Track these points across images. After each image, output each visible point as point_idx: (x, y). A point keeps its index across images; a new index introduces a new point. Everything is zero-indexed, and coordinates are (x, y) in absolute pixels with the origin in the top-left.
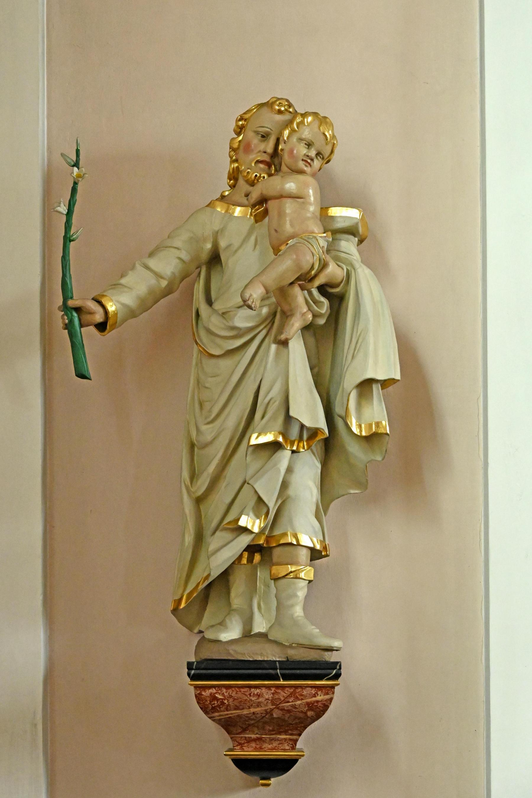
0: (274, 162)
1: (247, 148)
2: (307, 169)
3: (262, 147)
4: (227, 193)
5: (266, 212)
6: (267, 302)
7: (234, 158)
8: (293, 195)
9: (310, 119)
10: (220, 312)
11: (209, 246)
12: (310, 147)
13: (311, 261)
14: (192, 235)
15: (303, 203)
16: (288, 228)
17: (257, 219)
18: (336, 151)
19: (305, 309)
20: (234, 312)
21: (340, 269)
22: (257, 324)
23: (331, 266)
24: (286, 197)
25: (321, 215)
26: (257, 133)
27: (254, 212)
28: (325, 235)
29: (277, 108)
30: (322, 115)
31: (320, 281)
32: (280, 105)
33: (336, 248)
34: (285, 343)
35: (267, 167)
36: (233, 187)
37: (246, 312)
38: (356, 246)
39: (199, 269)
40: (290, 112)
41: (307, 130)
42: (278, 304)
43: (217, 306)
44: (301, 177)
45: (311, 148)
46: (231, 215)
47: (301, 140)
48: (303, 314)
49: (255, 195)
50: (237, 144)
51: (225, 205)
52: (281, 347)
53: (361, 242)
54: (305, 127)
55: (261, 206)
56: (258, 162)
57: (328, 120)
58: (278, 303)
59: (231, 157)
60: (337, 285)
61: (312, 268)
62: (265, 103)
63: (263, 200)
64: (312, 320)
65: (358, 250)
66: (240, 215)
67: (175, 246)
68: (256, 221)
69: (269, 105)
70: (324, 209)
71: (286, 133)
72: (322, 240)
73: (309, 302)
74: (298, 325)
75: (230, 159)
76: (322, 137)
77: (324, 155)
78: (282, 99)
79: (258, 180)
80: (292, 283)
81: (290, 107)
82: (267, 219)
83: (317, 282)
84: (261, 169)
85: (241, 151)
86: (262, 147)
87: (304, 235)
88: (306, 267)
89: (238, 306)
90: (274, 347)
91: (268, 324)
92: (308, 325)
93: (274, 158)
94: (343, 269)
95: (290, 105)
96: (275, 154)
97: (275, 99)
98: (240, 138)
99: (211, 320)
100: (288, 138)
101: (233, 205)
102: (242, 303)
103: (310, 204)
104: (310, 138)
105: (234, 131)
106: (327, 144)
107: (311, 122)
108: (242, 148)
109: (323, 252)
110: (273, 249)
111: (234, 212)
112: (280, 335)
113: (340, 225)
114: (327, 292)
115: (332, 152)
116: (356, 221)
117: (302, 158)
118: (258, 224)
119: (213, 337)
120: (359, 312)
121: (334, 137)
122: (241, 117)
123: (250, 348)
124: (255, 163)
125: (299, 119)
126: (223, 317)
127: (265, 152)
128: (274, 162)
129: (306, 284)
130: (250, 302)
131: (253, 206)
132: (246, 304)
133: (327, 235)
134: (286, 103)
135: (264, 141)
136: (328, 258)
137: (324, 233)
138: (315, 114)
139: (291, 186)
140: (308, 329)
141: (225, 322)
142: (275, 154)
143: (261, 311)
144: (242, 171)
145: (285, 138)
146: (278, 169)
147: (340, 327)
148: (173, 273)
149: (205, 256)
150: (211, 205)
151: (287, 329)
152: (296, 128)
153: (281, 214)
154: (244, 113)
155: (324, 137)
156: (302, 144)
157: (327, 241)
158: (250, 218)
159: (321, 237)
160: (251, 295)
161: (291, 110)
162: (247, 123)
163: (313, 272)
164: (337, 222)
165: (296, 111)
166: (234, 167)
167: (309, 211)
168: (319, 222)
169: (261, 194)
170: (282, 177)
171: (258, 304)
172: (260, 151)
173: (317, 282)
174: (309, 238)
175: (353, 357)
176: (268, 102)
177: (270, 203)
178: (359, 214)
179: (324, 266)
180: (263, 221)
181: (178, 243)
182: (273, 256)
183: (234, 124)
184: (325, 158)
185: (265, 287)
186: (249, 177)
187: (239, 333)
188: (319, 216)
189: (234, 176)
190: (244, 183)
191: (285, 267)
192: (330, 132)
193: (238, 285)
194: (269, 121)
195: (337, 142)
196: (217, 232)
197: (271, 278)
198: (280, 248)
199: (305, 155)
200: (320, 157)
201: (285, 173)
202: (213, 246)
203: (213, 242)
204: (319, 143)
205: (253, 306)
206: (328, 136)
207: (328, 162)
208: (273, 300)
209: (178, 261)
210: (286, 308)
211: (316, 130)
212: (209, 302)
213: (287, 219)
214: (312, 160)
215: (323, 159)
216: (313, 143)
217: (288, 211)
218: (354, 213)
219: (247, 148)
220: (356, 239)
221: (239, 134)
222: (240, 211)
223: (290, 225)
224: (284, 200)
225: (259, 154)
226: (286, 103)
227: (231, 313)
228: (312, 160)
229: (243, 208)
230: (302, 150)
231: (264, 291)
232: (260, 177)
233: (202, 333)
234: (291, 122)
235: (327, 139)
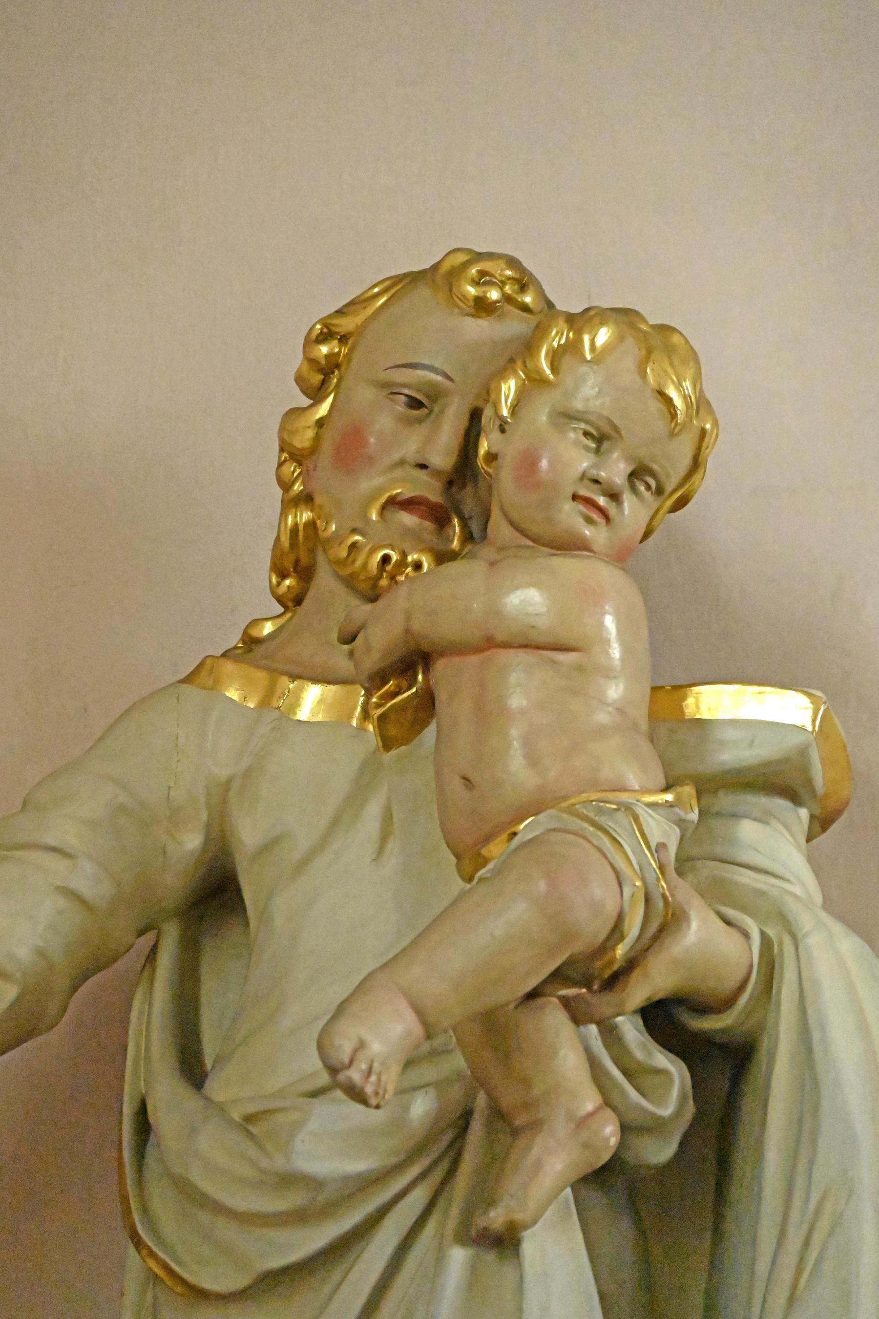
0: (459, 502)
1: (349, 447)
2: (596, 534)
3: (411, 445)
4: (268, 628)
5: (427, 705)
6: (429, 1072)
7: (298, 487)
8: (541, 639)
9: (603, 335)
10: (236, 1115)
11: (192, 841)
12: (606, 445)
13: (611, 908)
14: (123, 798)
15: (580, 668)
16: (518, 770)
17: (392, 731)
18: (712, 462)
19: (590, 1101)
20: (294, 1116)
21: (737, 936)
22: (394, 1160)
23: (694, 925)
24: (506, 645)
25: (653, 716)
26: (390, 389)
27: (378, 706)
28: (669, 797)
29: (472, 291)
30: (652, 322)
31: (654, 982)
32: (483, 279)
33: (719, 850)
34: (505, 1242)
35: (429, 525)
36: (293, 602)
37: (342, 1112)
38: (803, 840)
39: (150, 936)
40: (525, 308)
41: (591, 380)
42: (478, 1080)
43: (215, 1088)
44: (569, 567)
45: (610, 451)
46: (285, 718)
47: (566, 417)
48: (583, 1122)
49: (382, 636)
50: (310, 433)
51: (261, 676)
52: (490, 1257)
53: (822, 822)
54: (584, 369)
55: (408, 682)
56: (393, 503)
57: (676, 339)
58: (475, 1077)
59: (285, 485)
60: (729, 1002)
61: (617, 930)
62: (423, 272)
63: (414, 660)
64: (622, 1145)
65: (811, 860)
66: (320, 718)
67: (52, 842)
68: (387, 744)
69: (440, 278)
70: (665, 697)
71: (509, 388)
72: (657, 820)
73: (607, 1073)
74: (559, 1167)
75: (278, 492)
76: (655, 405)
77: (663, 479)
78: (490, 256)
79: (393, 578)
80: (533, 995)
81: (523, 288)
82: (430, 733)
83: (640, 991)
84: (407, 532)
85: (325, 458)
86: (411, 445)
87: (584, 796)
88: (595, 930)
89: (309, 1086)
90: (459, 1256)
91: (435, 1163)
92: (604, 1168)
93: (463, 487)
94: (746, 935)
95: (524, 282)
96: (465, 470)
97: (461, 258)
98: (324, 409)
99: (196, 1141)
100: (514, 409)
101: (294, 677)
102: (324, 1078)
103: (608, 673)
104: (606, 413)
105: (300, 380)
106: (672, 435)
107: (608, 348)
108: (327, 446)
109: (662, 867)
110: (457, 856)
111: (295, 705)
112: (486, 1212)
113: (731, 755)
114: (682, 1029)
115: (696, 464)
116: (793, 741)
117: (570, 491)
118: (394, 752)
119: (204, 1217)
120: (816, 1108)
121: (700, 405)
122: (325, 325)
123: (367, 1255)
124: (384, 507)
125: (558, 336)
126: (251, 1136)
127: (423, 466)
128: (459, 502)
129: (594, 999)
130: (355, 1075)
131: (376, 680)
132: (339, 1081)
133: (678, 798)
134: (509, 273)
135: (420, 421)
136: (684, 892)
137: (667, 789)
138: (626, 317)
139: (527, 600)
140: (607, 1180)
141: (252, 1151)
142: (465, 470)
143: (406, 1108)
144: (328, 541)
145: (505, 412)
146: (475, 527)
147: (735, 1192)
148: (41, 953)
149: (174, 882)
150: (204, 673)
151: (512, 1184)
152: (548, 371)
153: (489, 714)
154: (340, 312)
155: (662, 407)
156: (572, 435)
157: (681, 823)
158: (361, 728)
159: (653, 805)
160: (361, 1045)
161: (528, 299)
162: (352, 350)
163: (620, 951)
164: (722, 743)
165: (550, 305)
166: (296, 525)
167: (603, 702)
168: (645, 746)
169: (407, 631)
170: (492, 564)
171: (391, 1079)
172: (402, 463)
173: (640, 991)
174: (600, 811)
175: (792, 1299)
176: (436, 267)
177: (440, 666)
178: (810, 713)
179: (666, 923)
180: (416, 742)
181: (63, 830)
182: (460, 885)
183: (300, 356)
184: (669, 488)
185: (419, 1012)
186: (359, 562)
187: (316, 1199)
188: (644, 725)
189: (298, 563)
190: (339, 589)
191: (504, 930)
192: (687, 384)
193: (306, 1004)
194: (441, 342)
195: (715, 423)
196: (227, 785)
197: (450, 970)
198: (484, 852)
199: (583, 477)
200: (648, 487)
201: (501, 549)
202: (207, 840)
203: (208, 826)
204: (642, 425)
205: (369, 1089)
206: (678, 402)
207: (681, 503)
208: (458, 1062)
209: (62, 902)
210: (508, 1099)
211: (627, 375)
212: (193, 1070)
213: (514, 732)
214: (614, 497)
215: (659, 491)
216: (616, 429)
217: (517, 701)
218: (789, 709)
219: (349, 447)
220: (804, 813)
221: (316, 395)
222: (321, 701)
223: (526, 756)
224: (504, 656)
225: (398, 473)
226: (509, 273)
227: (280, 1118)
228: (614, 497)
229: (332, 688)
230: (573, 458)
231: (418, 1030)
232: (402, 563)
233: (162, 1202)
234: (528, 346)
235: (673, 416)
